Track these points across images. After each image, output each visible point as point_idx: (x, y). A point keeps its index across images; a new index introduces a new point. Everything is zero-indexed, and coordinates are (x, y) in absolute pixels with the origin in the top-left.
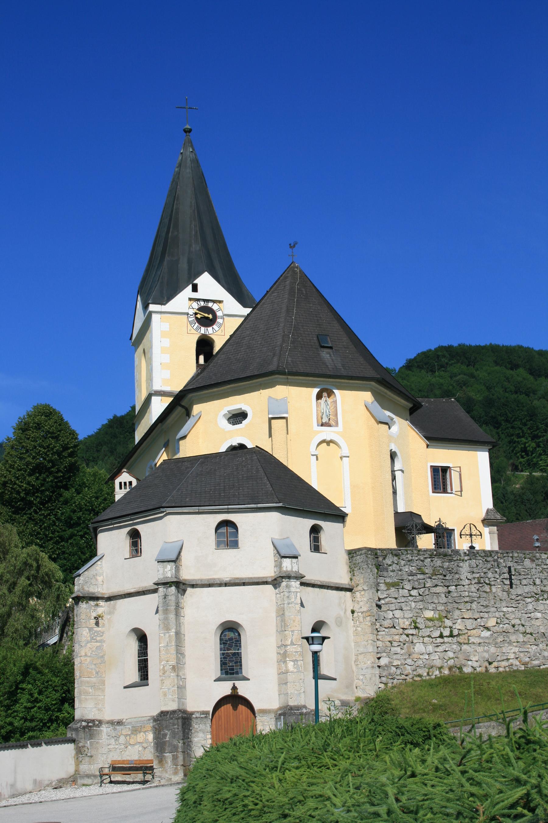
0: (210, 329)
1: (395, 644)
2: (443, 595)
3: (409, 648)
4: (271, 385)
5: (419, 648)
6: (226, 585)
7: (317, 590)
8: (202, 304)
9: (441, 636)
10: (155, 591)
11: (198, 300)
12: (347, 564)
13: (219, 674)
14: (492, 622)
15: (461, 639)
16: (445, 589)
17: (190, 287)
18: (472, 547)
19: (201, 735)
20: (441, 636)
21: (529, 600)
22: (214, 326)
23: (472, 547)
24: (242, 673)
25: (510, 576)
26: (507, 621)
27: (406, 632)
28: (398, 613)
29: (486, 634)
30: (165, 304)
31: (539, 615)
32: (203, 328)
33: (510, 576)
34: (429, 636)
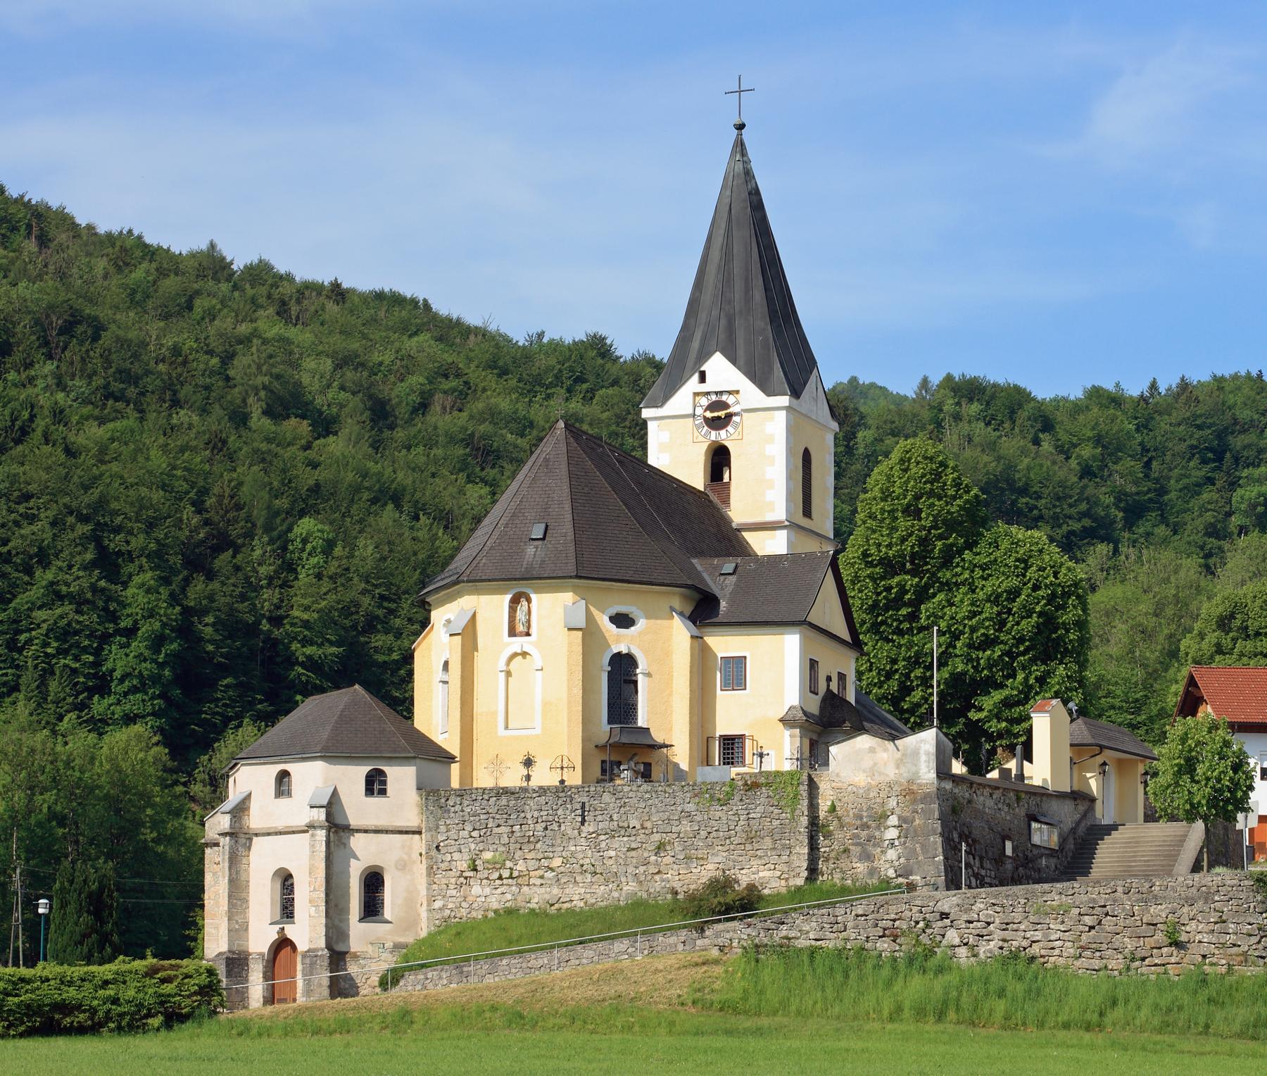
0: (723, 432)
1: (452, 887)
2: (506, 836)
3: (466, 890)
4: (459, 595)
5: (476, 890)
6: (281, 833)
7: (371, 835)
8: (714, 398)
9: (500, 878)
10: (307, 831)
11: (708, 393)
12: (417, 805)
13: (278, 917)
14: (557, 862)
15: (520, 881)
16: (508, 829)
17: (696, 377)
18: (562, 782)
19: (255, 974)
20: (500, 878)
21: (603, 837)
22: (729, 428)
23: (562, 782)
24: (383, 914)
25: (583, 812)
26: (575, 861)
27: (464, 874)
28: (456, 856)
29: (549, 875)
30: (661, 406)
31: (612, 853)
32: (713, 433)
33: (583, 812)
34: (487, 878)
